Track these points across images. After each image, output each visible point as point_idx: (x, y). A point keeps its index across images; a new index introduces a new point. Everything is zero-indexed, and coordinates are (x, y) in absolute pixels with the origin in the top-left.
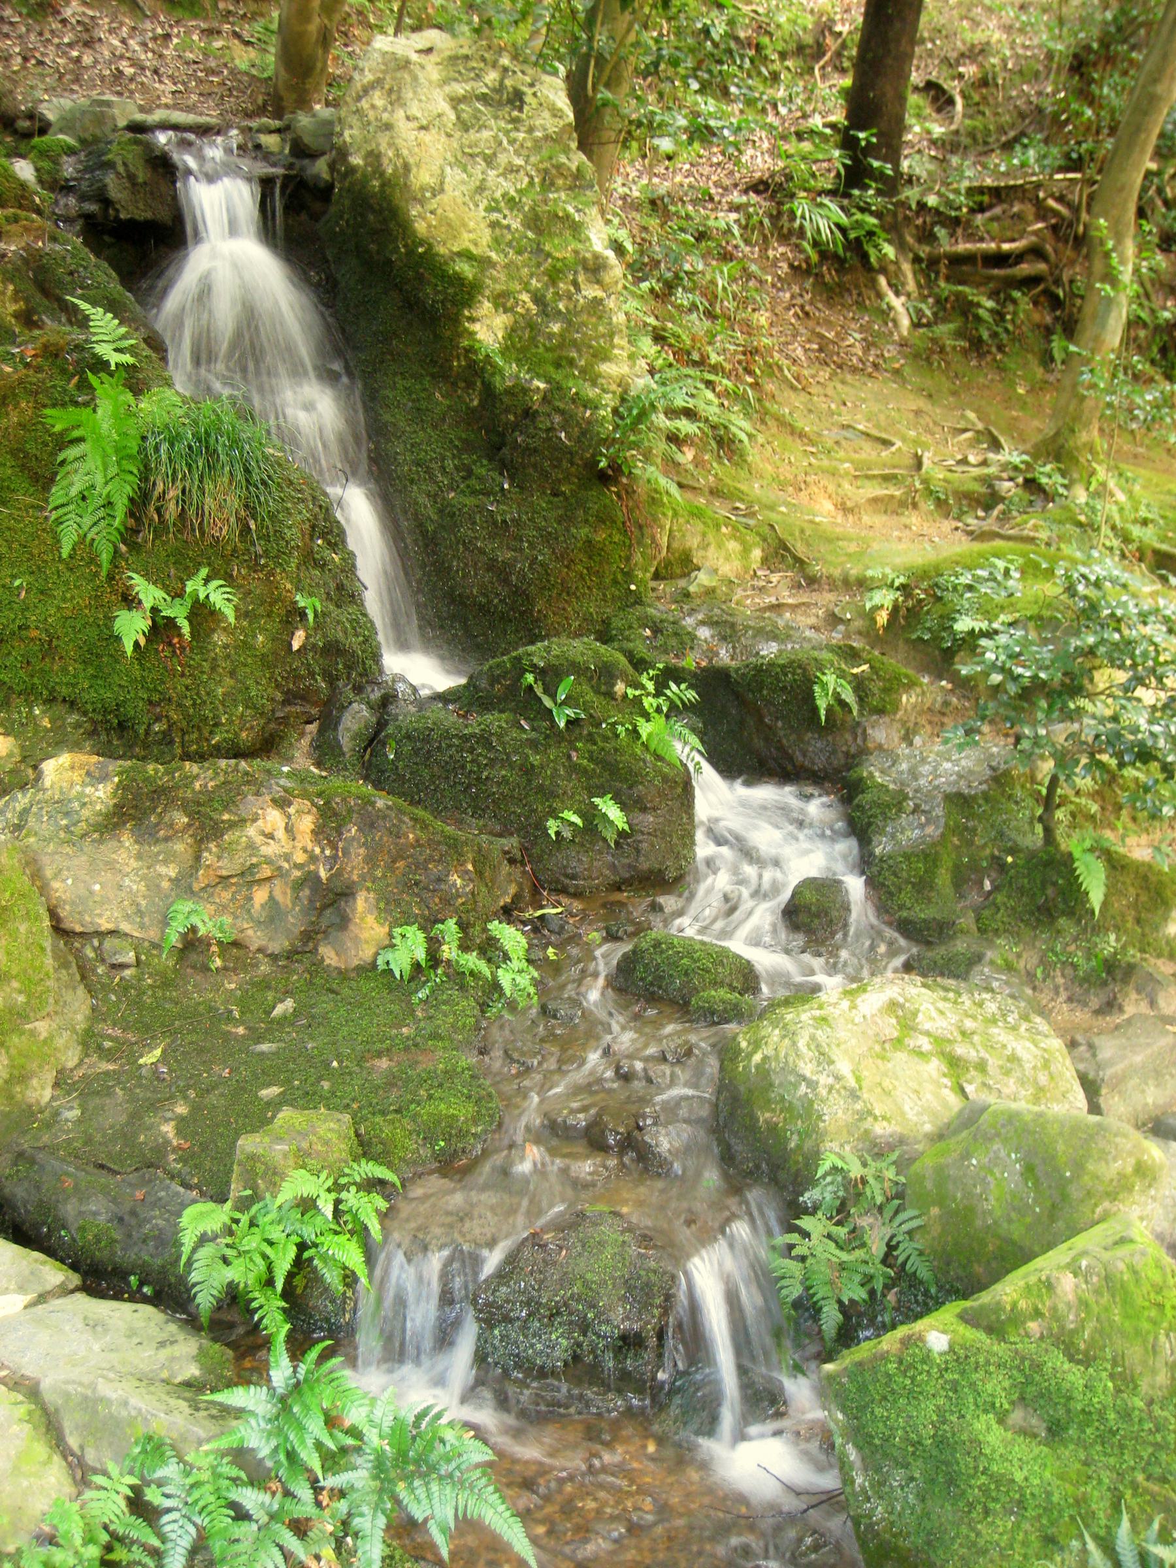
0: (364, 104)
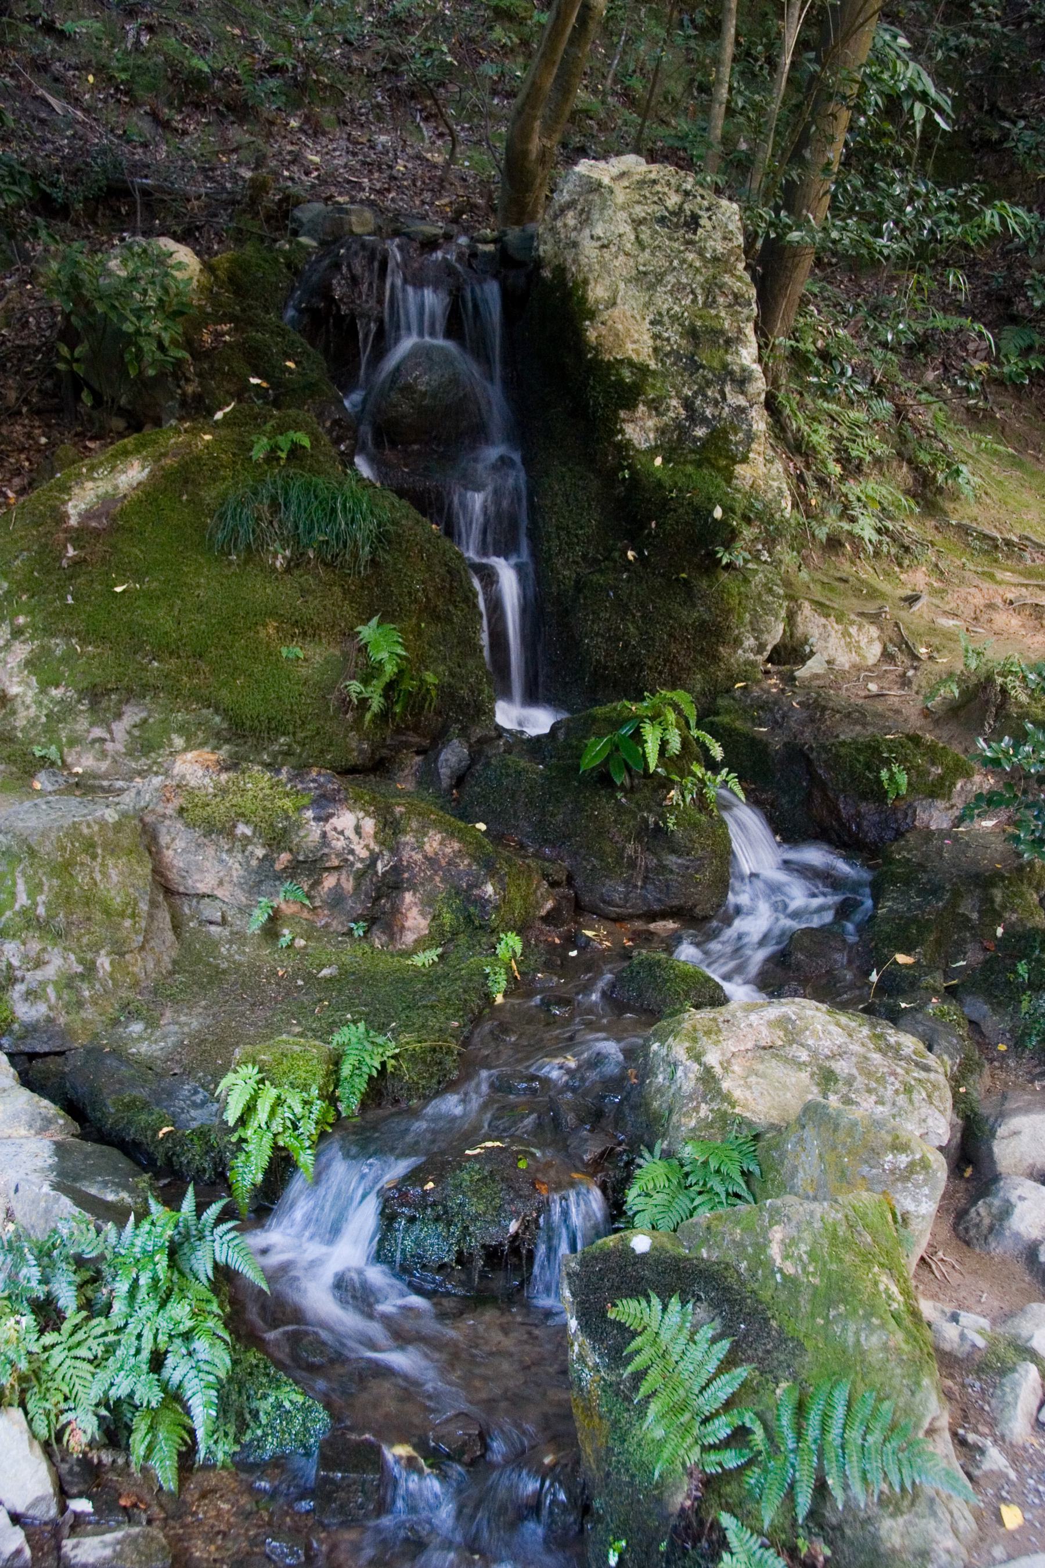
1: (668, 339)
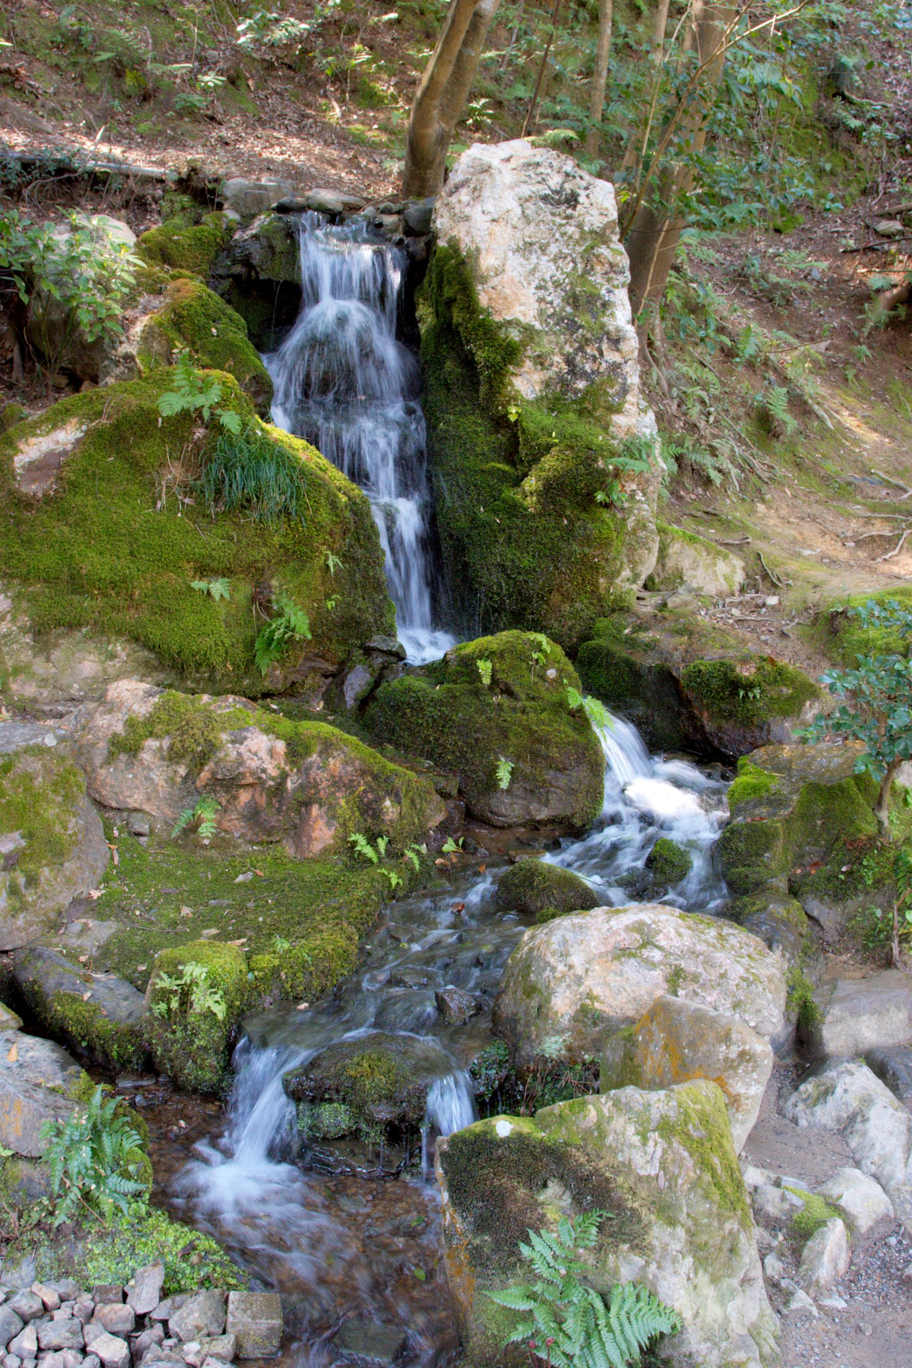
0: (453, 199)
1: (551, 303)
